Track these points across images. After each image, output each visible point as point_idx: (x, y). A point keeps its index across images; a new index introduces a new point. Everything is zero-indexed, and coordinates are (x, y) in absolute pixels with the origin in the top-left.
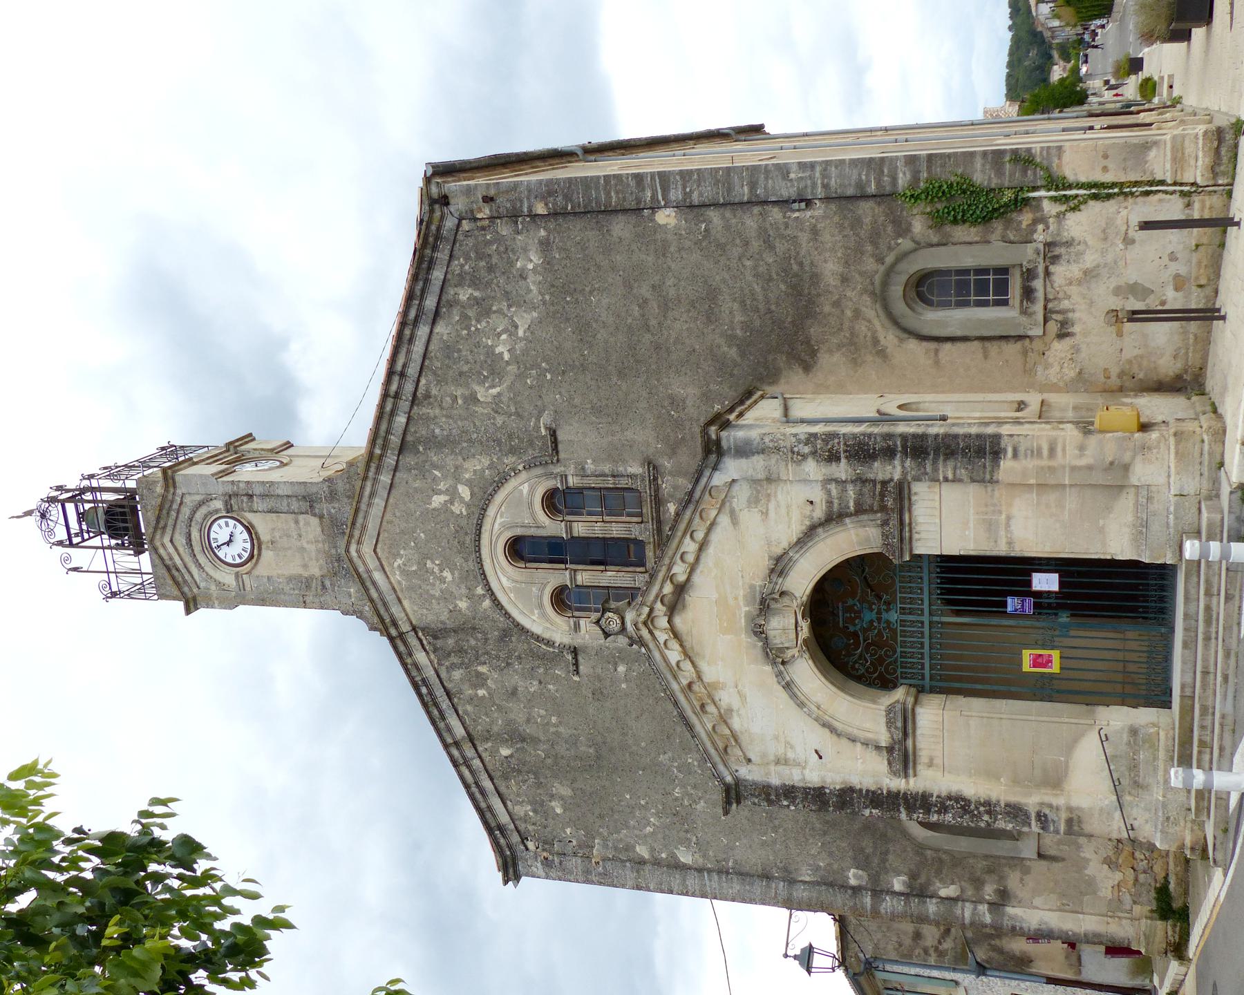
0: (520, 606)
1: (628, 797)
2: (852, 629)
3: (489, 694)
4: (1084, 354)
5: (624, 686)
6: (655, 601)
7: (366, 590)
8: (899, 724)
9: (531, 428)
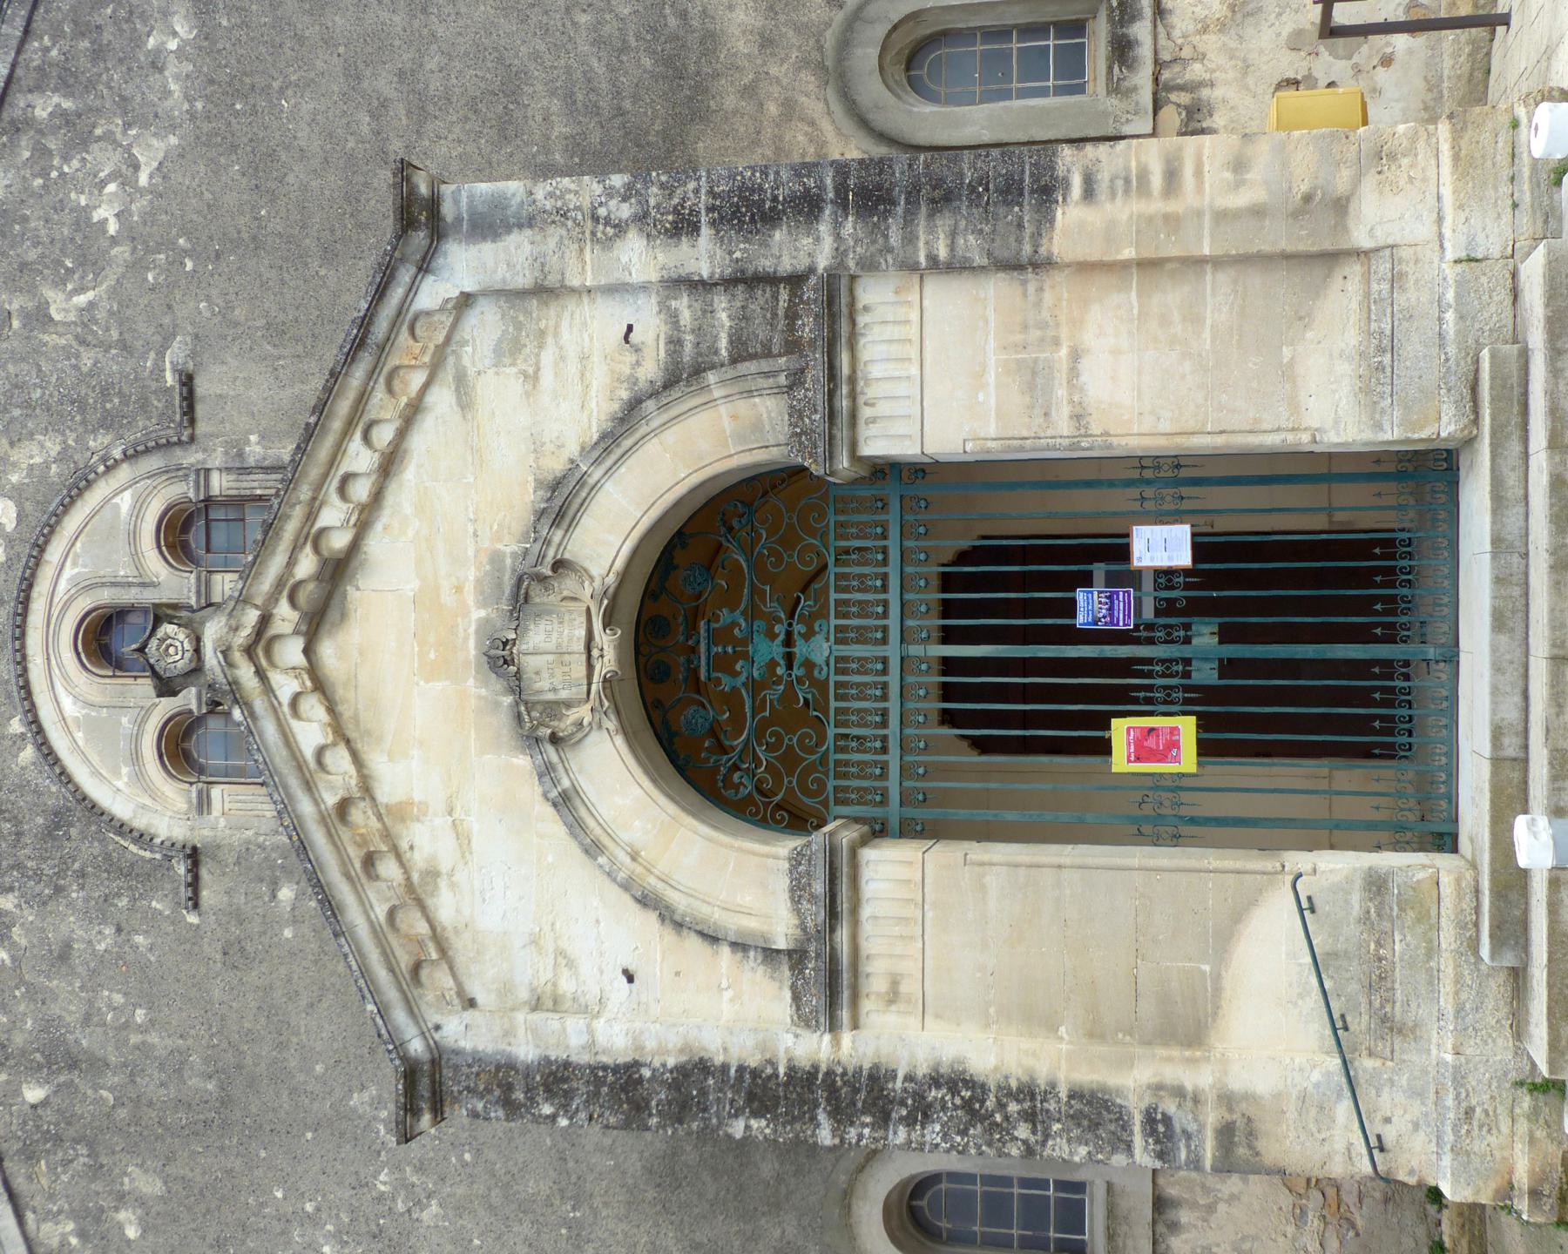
0: (94, 758)
1: (279, 1195)
2: (727, 683)
3: (13, 958)
5: (288, 933)
6: (273, 598)
8: (819, 887)
9: (147, 373)
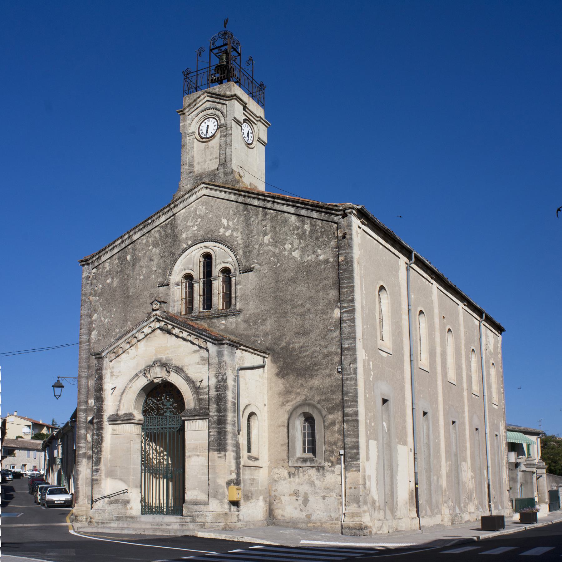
0: (184, 260)
4: (283, 482)
7: (188, 193)
8: (125, 418)
9: (253, 260)
